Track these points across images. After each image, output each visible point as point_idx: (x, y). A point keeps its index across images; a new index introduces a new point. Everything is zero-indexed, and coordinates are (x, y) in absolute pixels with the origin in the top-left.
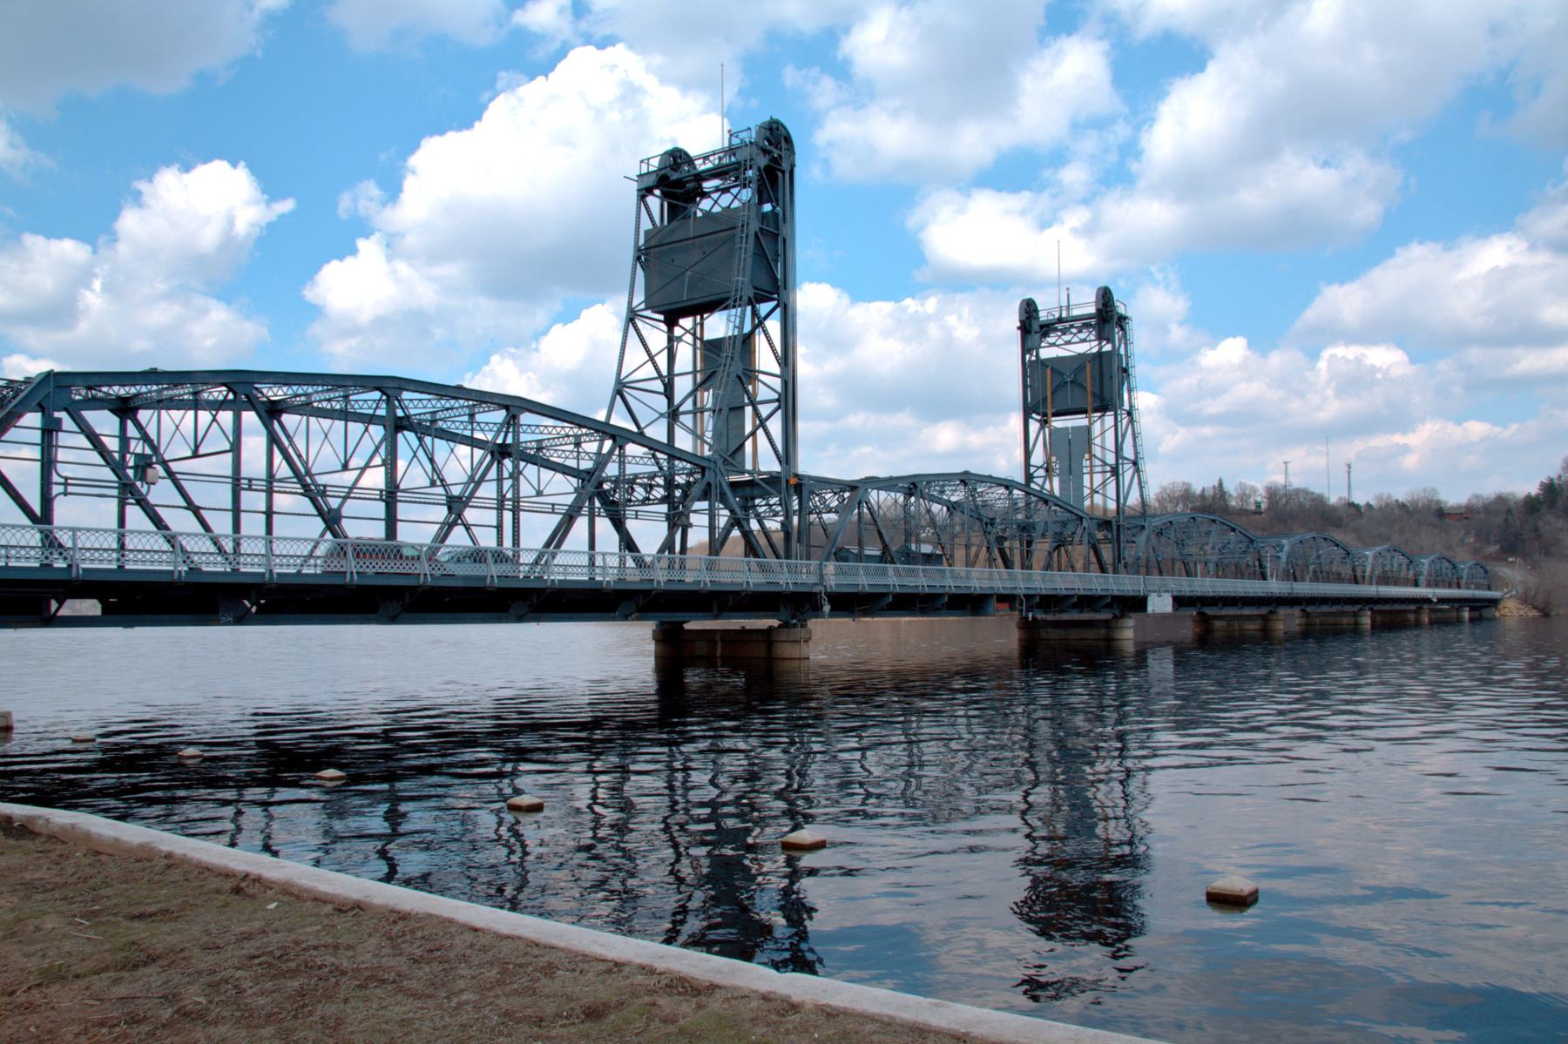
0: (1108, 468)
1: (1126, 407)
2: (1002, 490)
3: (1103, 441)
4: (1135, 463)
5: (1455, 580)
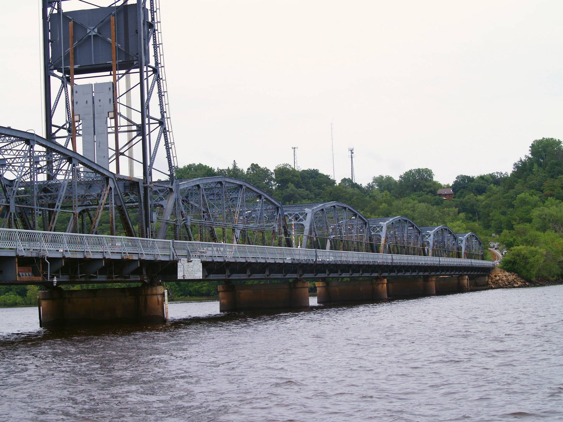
0: (134, 128)
1: (152, 63)
2: (21, 146)
3: (129, 100)
4: (161, 123)
5: (456, 251)
